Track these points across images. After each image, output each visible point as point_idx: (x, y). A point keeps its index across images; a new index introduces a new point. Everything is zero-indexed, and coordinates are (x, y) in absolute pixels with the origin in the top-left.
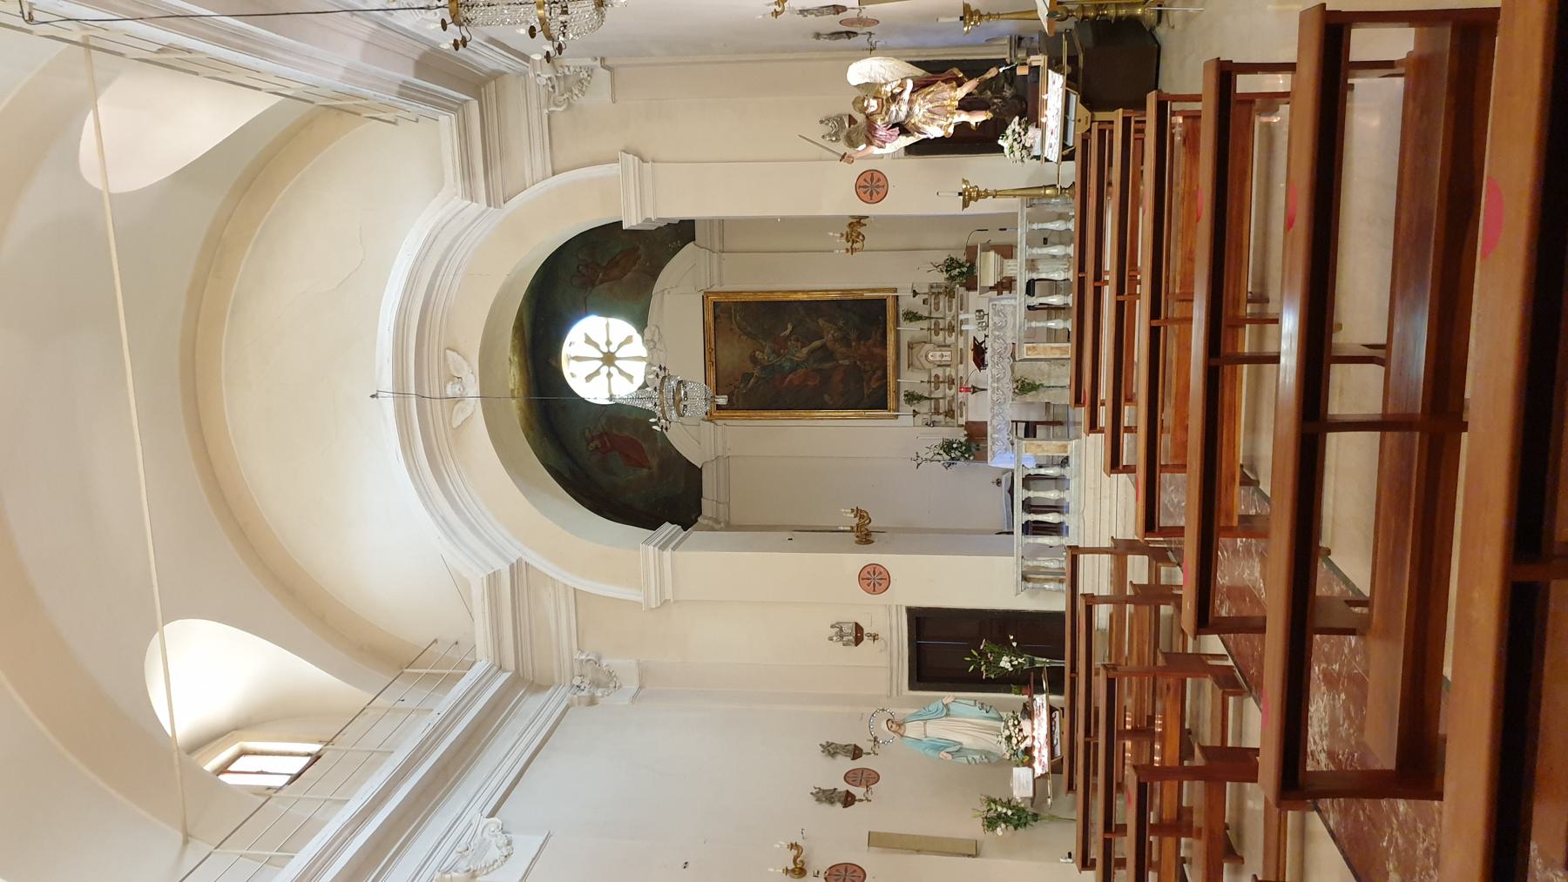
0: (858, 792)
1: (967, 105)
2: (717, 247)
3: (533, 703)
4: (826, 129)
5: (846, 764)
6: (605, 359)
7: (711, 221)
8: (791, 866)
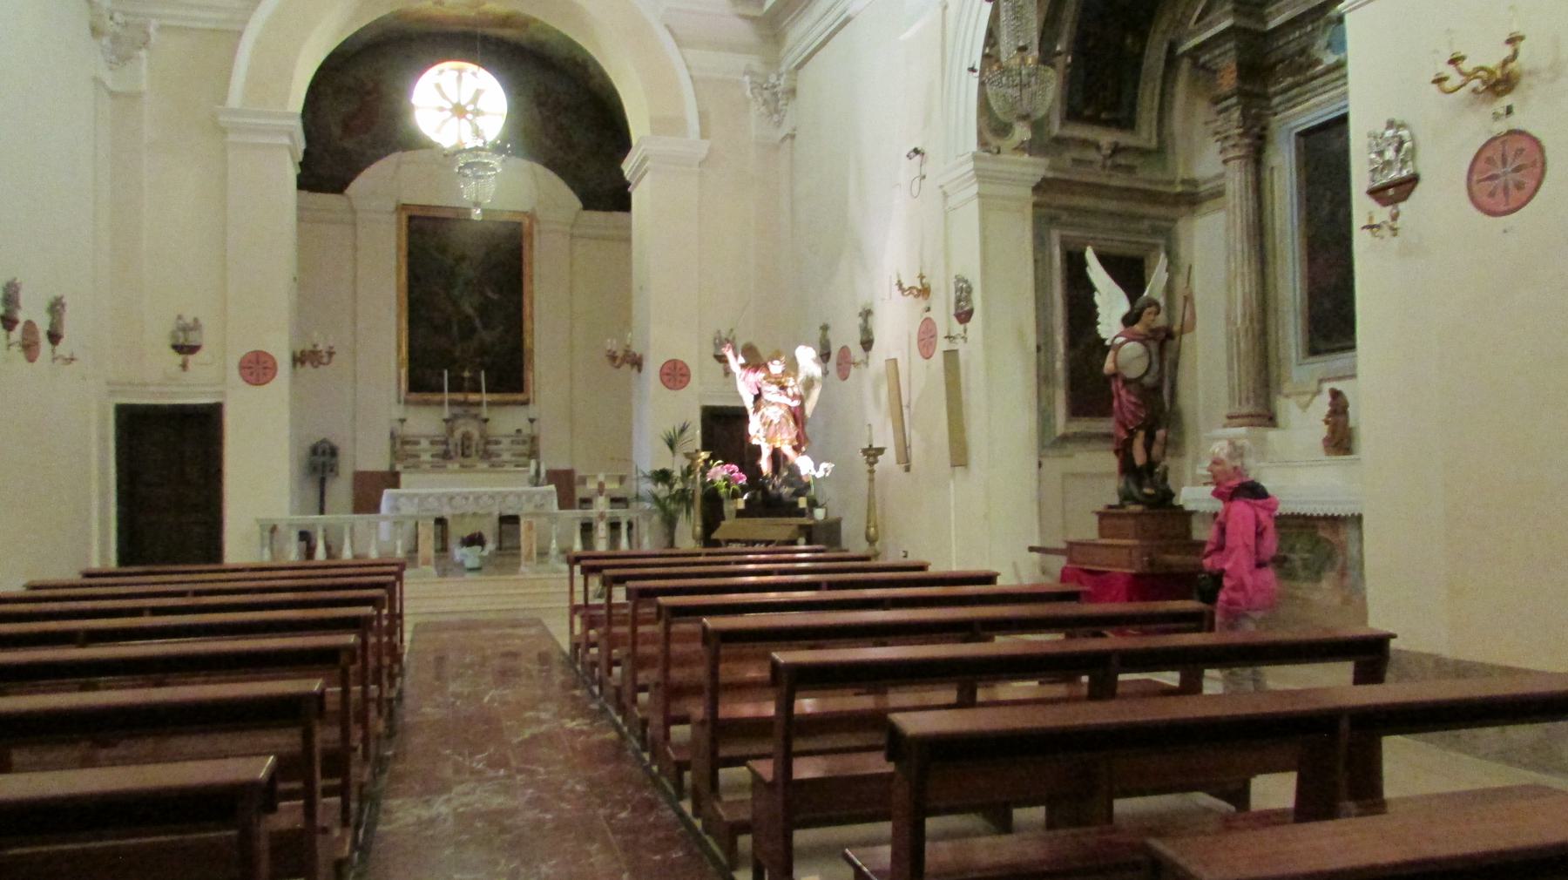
0: (16, 334)
1: (776, 456)
2: (576, 232)
5: (43, 324)
6: (459, 110)
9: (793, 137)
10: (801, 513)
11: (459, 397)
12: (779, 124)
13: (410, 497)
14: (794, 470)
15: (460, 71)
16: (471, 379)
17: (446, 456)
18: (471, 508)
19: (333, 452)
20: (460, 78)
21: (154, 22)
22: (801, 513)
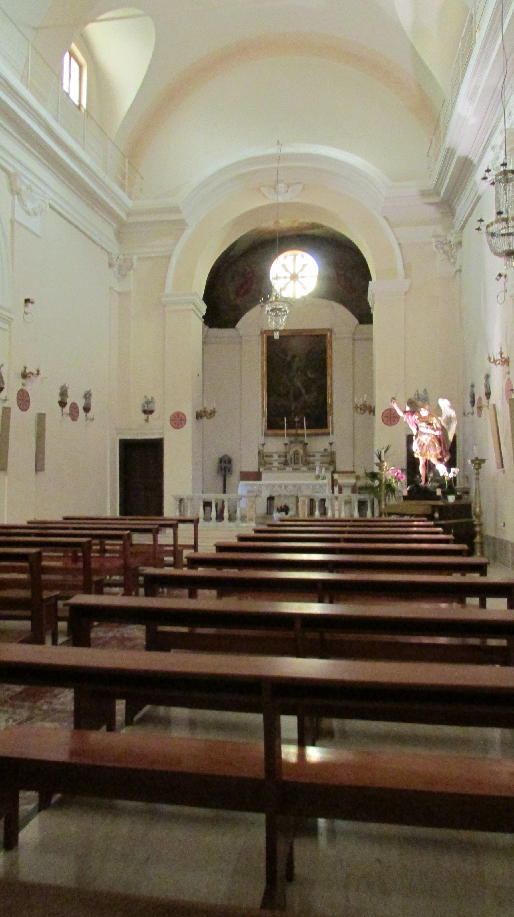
0: (67, 409)
2: (357, 336)
3: (110, 233)
4: (421, 392)
6: (295, 277)
7: (371, 333)
8: (28, 371)
9: (460, 271)
10: (438, 498)
11: (293, 431)
12: (454, 264)
13: (267, 486)
14: (437, 473)
15: (295, 256)
16: (298, 422)
17: (286, 463)
18: (283, 492)
19: (230, 461)
20: (295, 259)
21: (135, 258)
22: (438, 498)
